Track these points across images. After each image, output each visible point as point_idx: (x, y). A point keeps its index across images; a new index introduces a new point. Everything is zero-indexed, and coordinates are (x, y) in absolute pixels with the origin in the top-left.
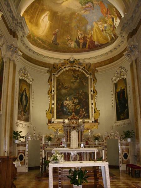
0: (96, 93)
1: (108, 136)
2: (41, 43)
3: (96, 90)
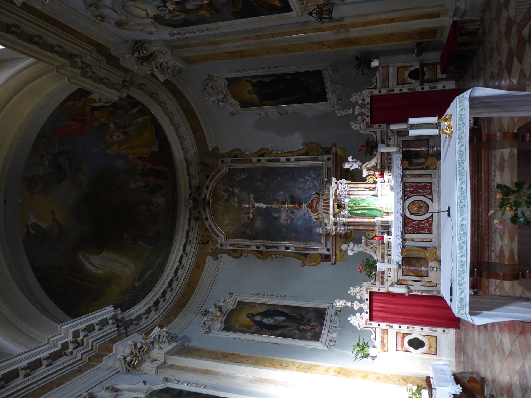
0: (264, 151)
1: (363, 121)
2: (151, 271)
3: (258, 152)
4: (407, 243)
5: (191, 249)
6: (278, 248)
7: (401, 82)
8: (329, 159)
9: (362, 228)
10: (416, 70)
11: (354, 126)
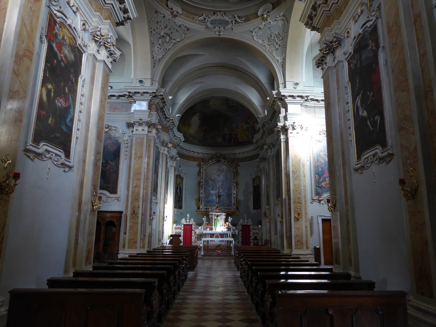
1: (243, 223)
2: (192, 139)
3: (238, 183)
4: (207, 235)
5: (201, 155)
6: (202, 190)
7: (254, 234)
8: (234, 209)
9: (211, 222)
10: (257, 238)
11: (241, 220)
